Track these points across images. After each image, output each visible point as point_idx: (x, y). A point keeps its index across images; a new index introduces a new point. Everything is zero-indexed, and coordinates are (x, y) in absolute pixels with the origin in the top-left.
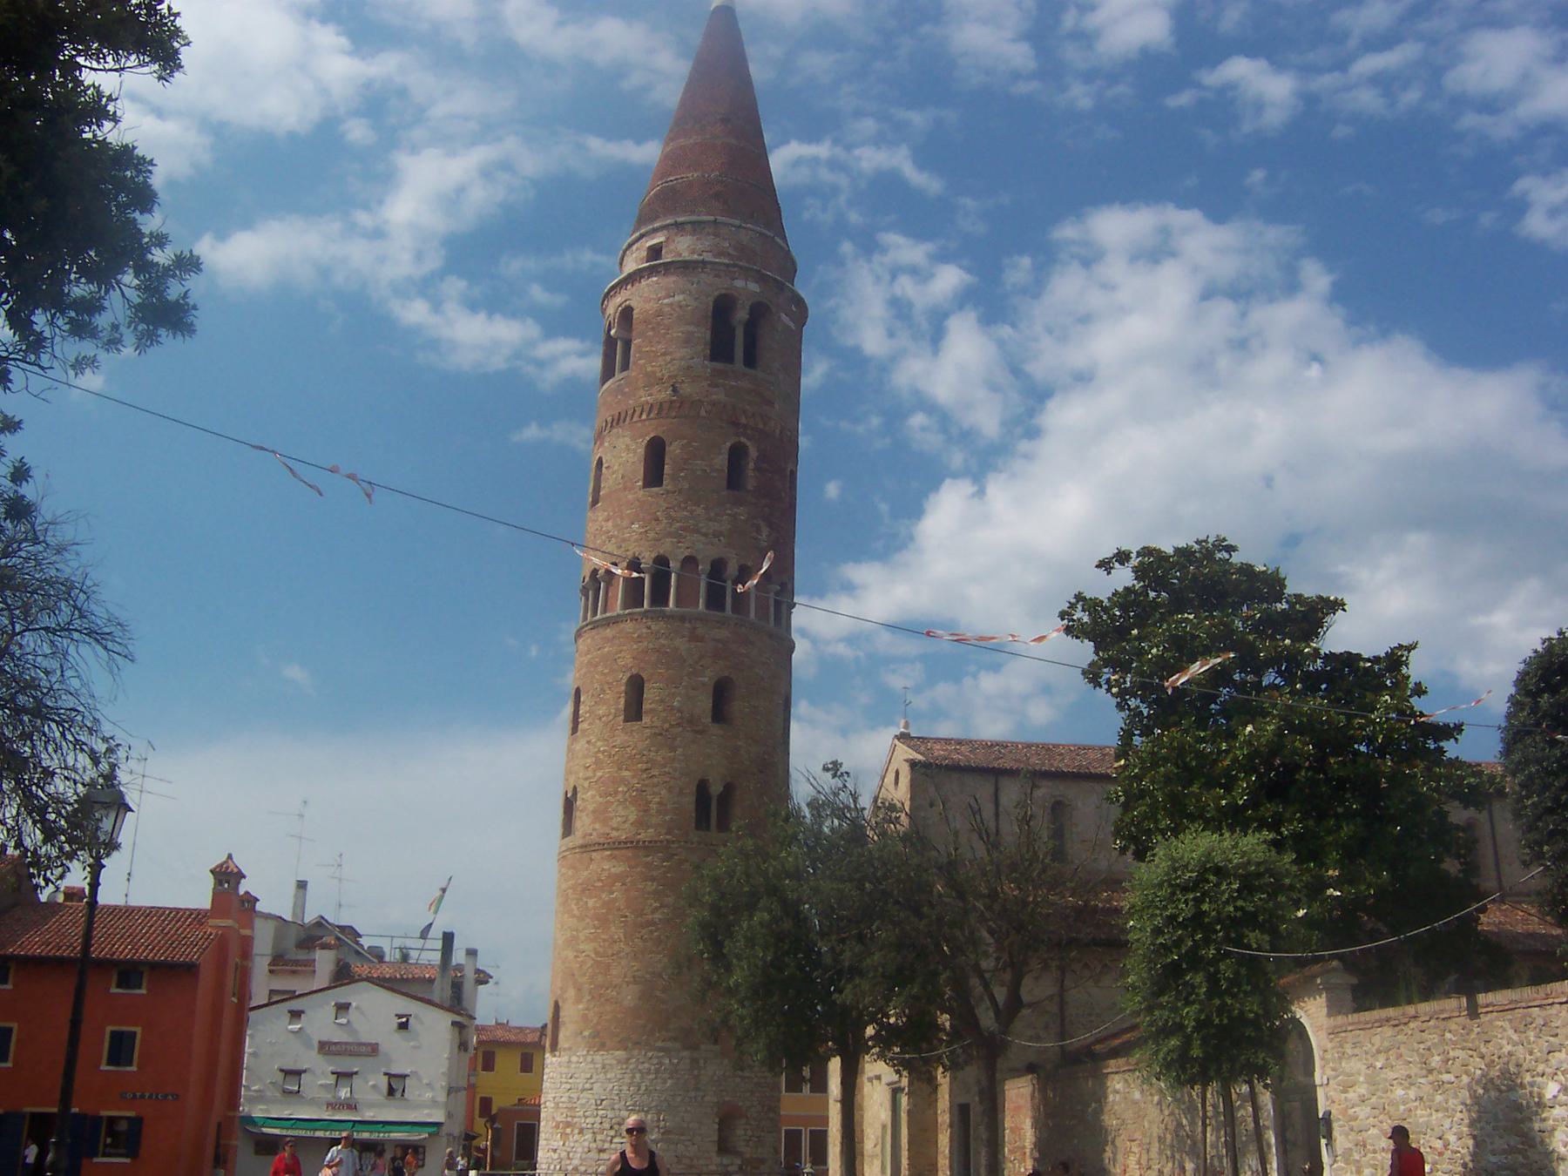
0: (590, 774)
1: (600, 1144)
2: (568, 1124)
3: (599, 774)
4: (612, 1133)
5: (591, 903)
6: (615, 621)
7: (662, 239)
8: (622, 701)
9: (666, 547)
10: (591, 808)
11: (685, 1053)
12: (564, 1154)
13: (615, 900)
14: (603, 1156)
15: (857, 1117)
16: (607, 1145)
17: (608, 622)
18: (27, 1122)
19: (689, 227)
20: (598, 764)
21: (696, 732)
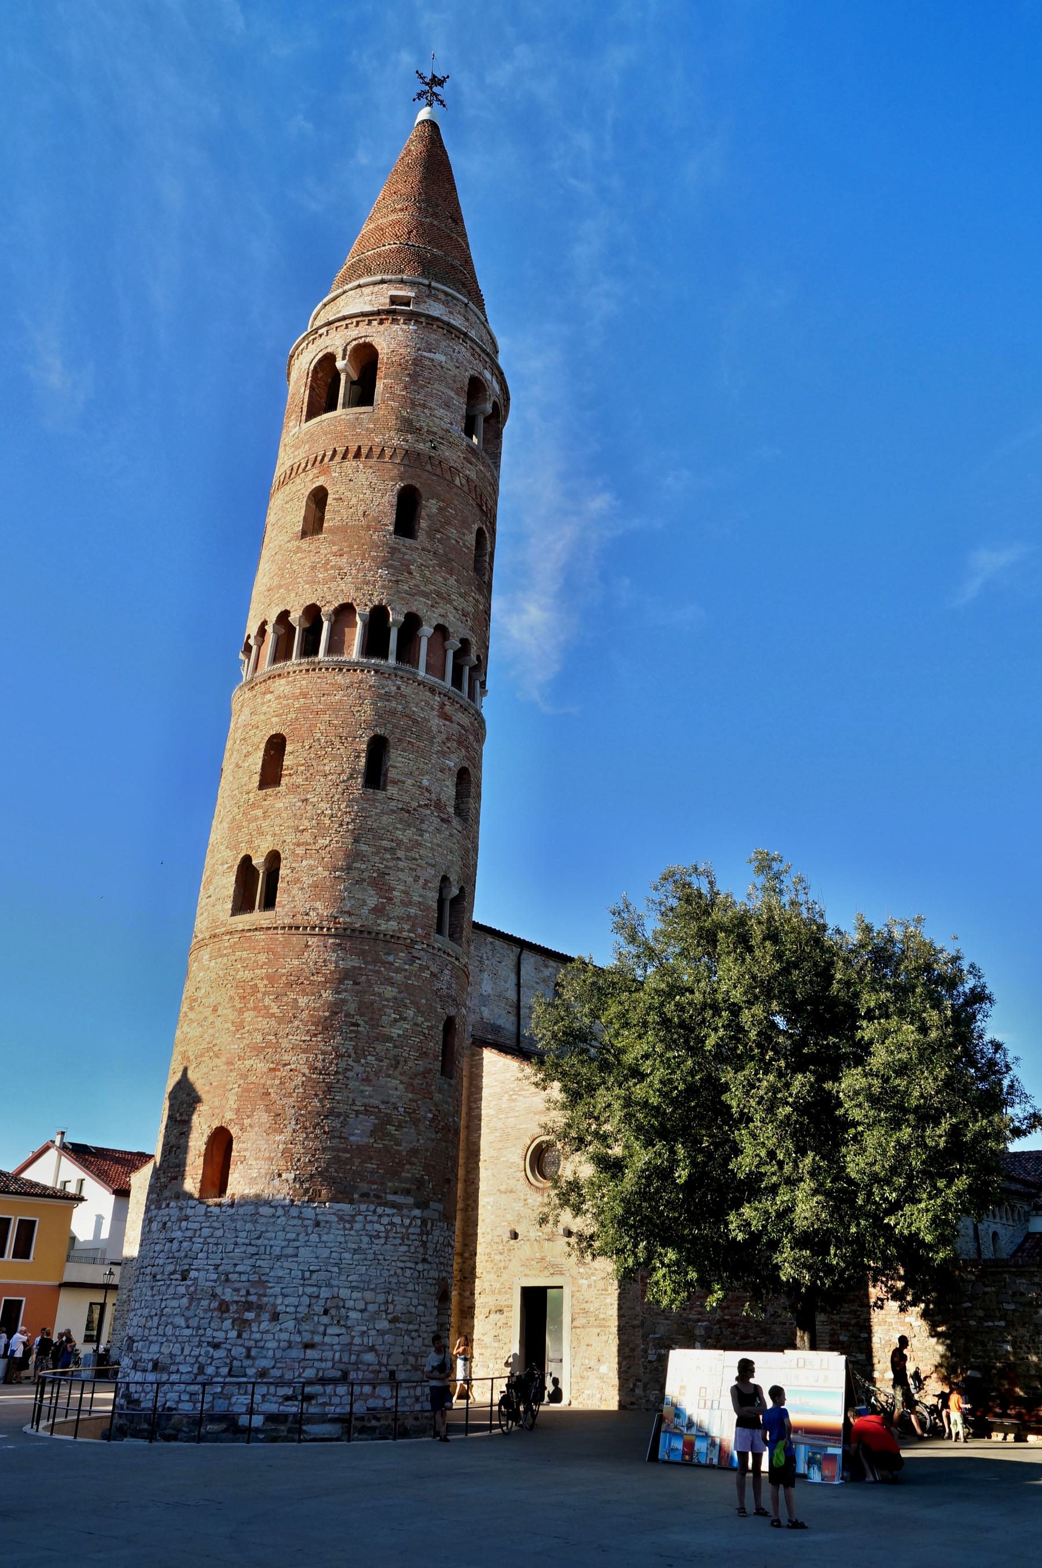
0: (307, 837)
1: (307, 1337)
2: (248, 1306)
3: (321, 842)
4: (325, 1320)
5: (303, 1001)
6: (353, 667)
7: (413, 295)
8: (363, 761)
9: (418, 606)
10: (307, 881)
11: (417, 1212)
12: (238, 1351)
13: (344, 1001)
14: (310, 1353)
15: (517, 1056)
16: (317, 1339)
17: (340, 667)
18: (340, 400)
19: (442, 296)
20: (321, 830)
21: (443, 820)
